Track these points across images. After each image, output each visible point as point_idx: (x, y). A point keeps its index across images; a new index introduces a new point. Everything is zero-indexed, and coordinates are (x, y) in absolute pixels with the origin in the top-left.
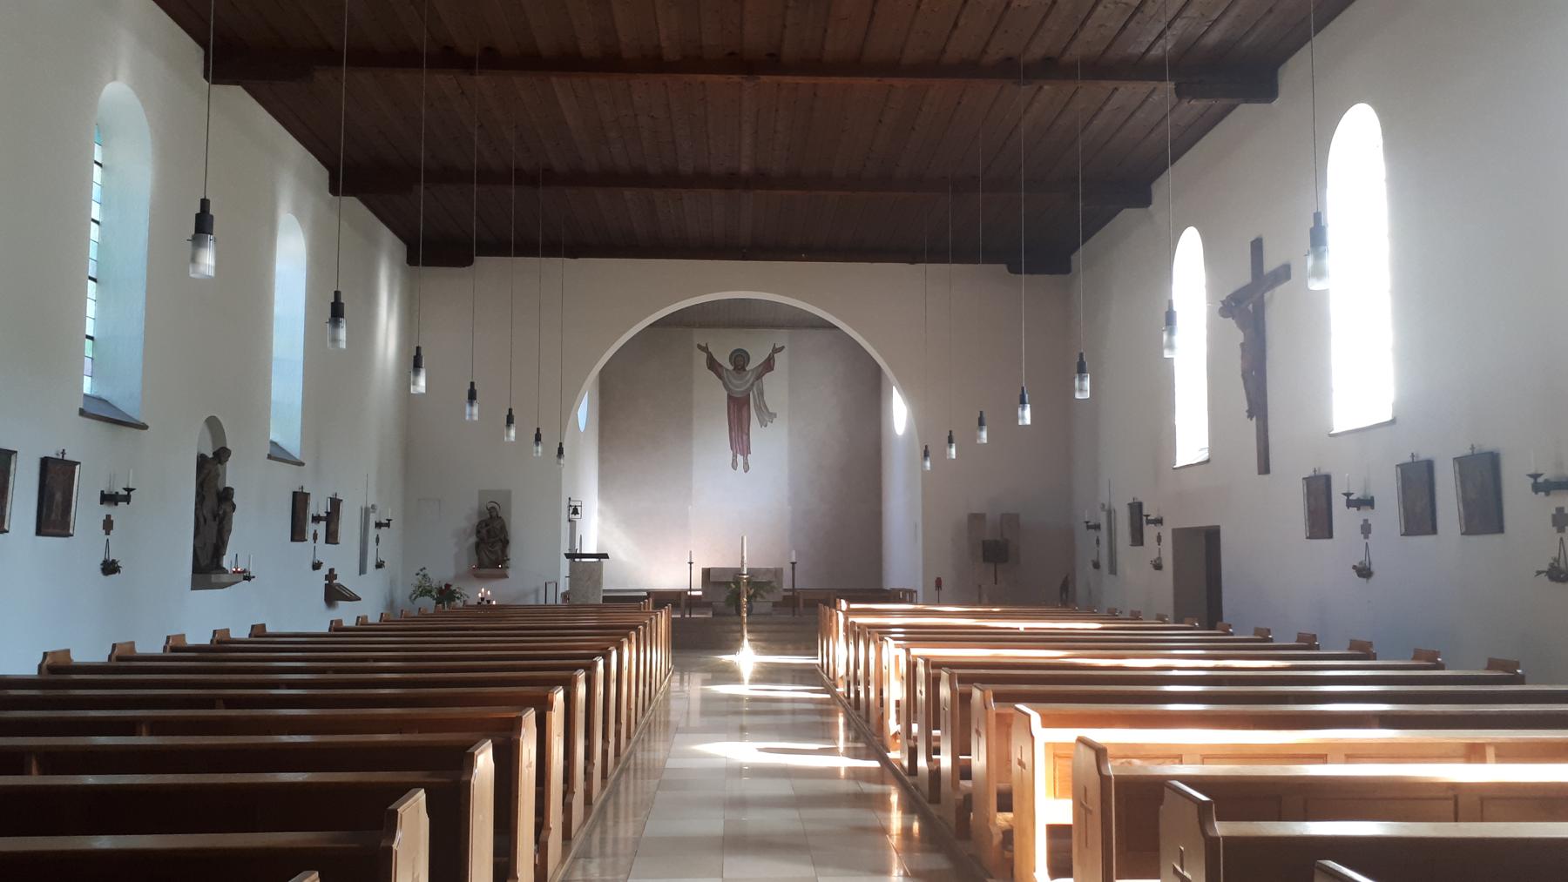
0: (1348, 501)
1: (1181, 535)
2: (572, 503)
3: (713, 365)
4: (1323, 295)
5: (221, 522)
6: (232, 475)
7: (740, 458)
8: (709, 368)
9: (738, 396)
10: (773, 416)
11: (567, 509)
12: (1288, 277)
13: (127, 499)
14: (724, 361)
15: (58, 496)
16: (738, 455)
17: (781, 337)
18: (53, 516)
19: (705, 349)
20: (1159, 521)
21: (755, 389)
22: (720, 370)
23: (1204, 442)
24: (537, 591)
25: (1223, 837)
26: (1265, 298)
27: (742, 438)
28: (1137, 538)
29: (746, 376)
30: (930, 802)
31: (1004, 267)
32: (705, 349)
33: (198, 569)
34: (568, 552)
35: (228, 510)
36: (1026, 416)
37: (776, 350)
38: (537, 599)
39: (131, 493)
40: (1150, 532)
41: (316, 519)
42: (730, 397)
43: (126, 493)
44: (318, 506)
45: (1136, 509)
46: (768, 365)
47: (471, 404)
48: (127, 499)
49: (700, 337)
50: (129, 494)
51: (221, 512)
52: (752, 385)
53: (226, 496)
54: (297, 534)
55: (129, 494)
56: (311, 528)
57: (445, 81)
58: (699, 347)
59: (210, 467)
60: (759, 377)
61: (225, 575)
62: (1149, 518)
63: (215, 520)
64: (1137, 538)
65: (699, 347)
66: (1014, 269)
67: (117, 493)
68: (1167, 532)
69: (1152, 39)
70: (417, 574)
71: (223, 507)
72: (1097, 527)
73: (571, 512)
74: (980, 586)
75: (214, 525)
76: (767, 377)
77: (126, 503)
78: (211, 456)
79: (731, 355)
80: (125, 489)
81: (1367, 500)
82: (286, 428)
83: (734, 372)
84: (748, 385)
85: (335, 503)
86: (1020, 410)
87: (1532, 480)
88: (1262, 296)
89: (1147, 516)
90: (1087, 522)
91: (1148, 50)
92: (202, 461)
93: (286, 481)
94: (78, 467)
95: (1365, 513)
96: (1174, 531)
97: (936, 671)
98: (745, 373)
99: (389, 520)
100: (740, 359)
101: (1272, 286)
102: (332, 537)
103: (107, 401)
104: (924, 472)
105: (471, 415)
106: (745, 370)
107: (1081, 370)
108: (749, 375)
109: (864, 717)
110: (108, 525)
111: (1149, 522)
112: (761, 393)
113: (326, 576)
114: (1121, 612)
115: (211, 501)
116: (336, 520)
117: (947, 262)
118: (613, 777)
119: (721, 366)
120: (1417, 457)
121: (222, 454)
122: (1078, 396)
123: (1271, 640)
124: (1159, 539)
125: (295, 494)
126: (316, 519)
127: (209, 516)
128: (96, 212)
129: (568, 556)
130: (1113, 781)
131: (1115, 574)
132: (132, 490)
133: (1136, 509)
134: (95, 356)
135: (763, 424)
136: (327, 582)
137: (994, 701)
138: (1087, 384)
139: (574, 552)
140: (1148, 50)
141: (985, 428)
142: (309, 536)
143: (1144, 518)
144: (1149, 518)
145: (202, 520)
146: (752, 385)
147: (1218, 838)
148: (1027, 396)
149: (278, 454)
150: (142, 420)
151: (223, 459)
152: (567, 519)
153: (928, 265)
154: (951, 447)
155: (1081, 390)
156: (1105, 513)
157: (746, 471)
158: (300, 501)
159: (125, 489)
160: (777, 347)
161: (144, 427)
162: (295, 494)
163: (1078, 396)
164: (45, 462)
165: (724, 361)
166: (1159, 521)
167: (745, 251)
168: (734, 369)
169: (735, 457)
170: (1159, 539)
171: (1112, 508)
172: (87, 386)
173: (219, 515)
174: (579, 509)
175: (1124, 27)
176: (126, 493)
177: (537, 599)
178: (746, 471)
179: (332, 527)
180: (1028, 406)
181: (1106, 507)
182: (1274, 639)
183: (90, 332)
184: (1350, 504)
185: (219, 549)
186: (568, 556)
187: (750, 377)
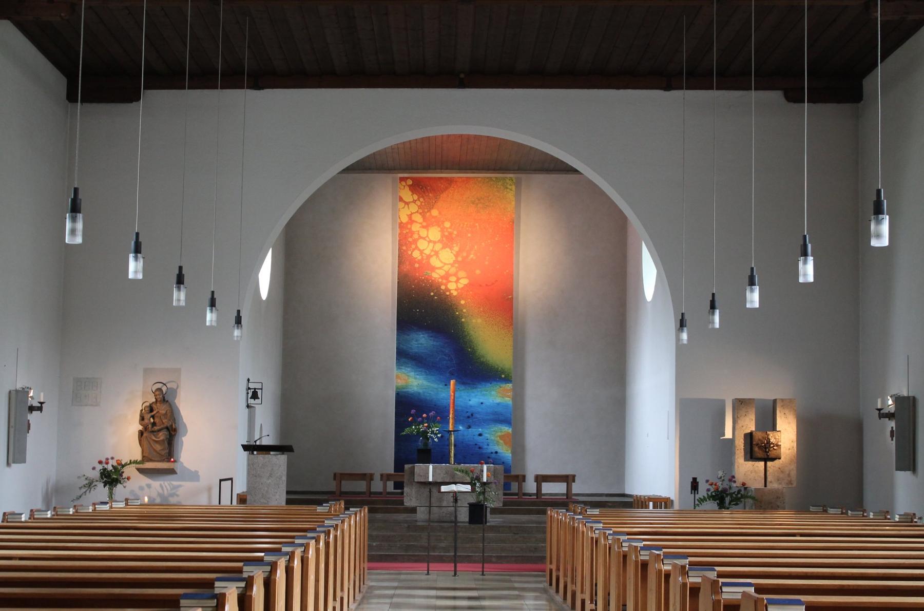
2: (251, 386)
4: (502, 368)
11: (245, 392)
24: (209, 489)
34: (246, 443)
36: (807, 271)
38: (210, 498)
39: (43, 405)
43: (40, 405)
47: (179, 289)
66: (794, 96)
70: (100, 462)
73: (250, 395)
74: (268, 435)
77: (40, 412)
86: (801, 264)
90: (879, 410)
99: (41, 403)
104: (257, 454)
105: (179, 300)
107: (878, 210)
117: (710, 88)
122: (874, 243)
132: (43, 403)
138: (885, 228)
139: (252, 443)
141: (757, 289)
148: (809, 246)
150: (260, 425)
152: (245, 405)
154: (713, 314)
163: (874, 243)
167: (462, 76)
174: (259, 392)
176: (40, 405)
177: (210, 498)
180: (810, 259)
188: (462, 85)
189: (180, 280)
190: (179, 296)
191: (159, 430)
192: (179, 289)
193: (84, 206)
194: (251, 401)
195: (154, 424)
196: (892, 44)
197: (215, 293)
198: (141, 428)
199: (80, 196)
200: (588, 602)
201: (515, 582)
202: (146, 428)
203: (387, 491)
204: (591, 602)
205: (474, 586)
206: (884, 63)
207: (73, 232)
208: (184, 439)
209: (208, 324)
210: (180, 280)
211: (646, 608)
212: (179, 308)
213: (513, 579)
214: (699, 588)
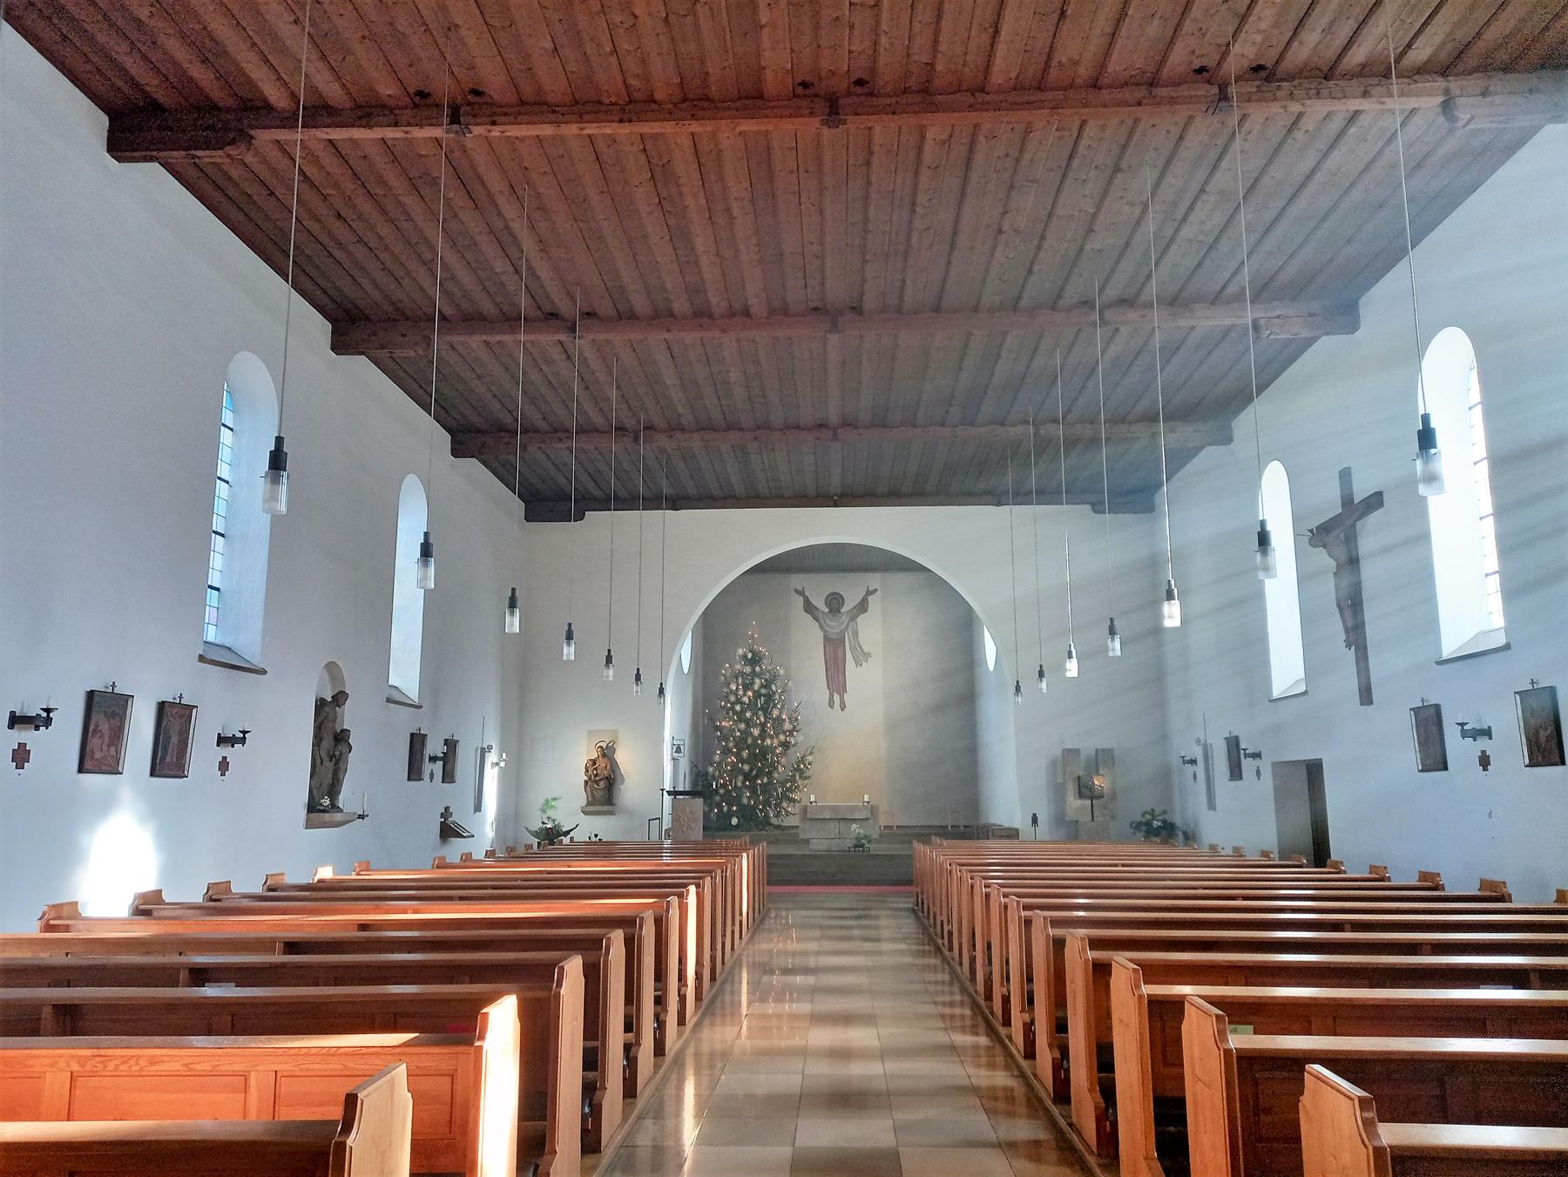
0: (1462, 730)
1: (1282, 768)
3: (809, 608)
5: (337, 763)
6: (350, 718)
7: (837, 698)
8: (806, 611)
9: (835, 637)
10: (867, 656)
12: (1381, 504)
13: (243, 741)
14: (819, 603)
15: (174, 739)
16: (835, 694)
17: (874, 580)
18: (168, 759)
19: (801, 593)
20: (1257, 755)
21: (850, 630)
22: (816, 612)
23: (1300, 673)
25: (1391, 1147)
26: (1357, 527)
27: (838, 677)
28: (1236, 772)
29: (841, 617)
30: (1026, 1057)
31: (1087, 508)
32: (801, 593)
33: (313, 807)
35: (344, 751)
37: (869, 593)
40: (1248, 765)
41: (433, 759)
42: (825, 638)
44: (434, 747)
45: (1233, 744)
46: (862, 607)
48: (243, 741)
49: (797, 581)
50: (48, 716)
51: (337, 753)
52: (848, 625)
53: (342, 738)
54: (414, 772)
55: (48, 716)
56: (428, 767)
57: (549, 339)
58: (796, 591)
59: (327, 710)
60: (853, 619)
61: (339, 814)
62: (1247, 752)
63: (331, 761)
64: (1236, 772)
65: (796, 591)
66: (1097, 508)
67: (234, 735)
68: (1266, 766)
69: (1227, 276)
71: (340, 748)
72: (1193, 762)
73: (675, 749)
75: (329, 765)
76: (861, 619)
78: (329, 699)
79: (829, 595)
80: (240, 731)
81: (1484, 730)
82: (405, 674)
83: (830, 615)
84: (844, 625)
85: (451, 745)
87: (1460, 727)
88: (1354, 525)
89: (1244, 750)
91: (1224, 288)
92: (321, 705)
93: (405, 724)
94: (195, 710)
95: (1482, 744)
96: (1274, 764)
97: (1028, 913)
98: (840, 615)
100: (835, 602)
101: (1363, 515)
102: (448, 776)
103: (229, 649)
105: (568, 654)
106: (840, 612)
108: (844, 617)
109: (958, 960)
110: (224, 766)
111: (1246, 756)
112: (856, 634)
113: (442, 814)
114: (1223, 849)
115: (327, 743)
116: (452, 760)
118: (693, 1023)
119: (817, 609)
120: (1537, 683)
121: (340, 698)
123: (1345, 872)
124: (1258, 773)
125: (412, 735)
126: (433, 759)
127: (325, 758)
128: (224, 470)
129: (669, 793)
130: (1235, 1056)
131: (1215, 810)
133: (1233, 744)
134: (220, 606)
135: (858, 664)
136: (443, 820)
137: (1090, 950)
140: (1224, 288)
142: (426, 776)
143: (1242, 752)
144: (1247, 752)
145: (319, 761)
146: (848, 625)
147: (1384, 1149)
149: (395, 700)
151: (340, 702)
153: (1013, 507)
155: (1170, 617)
156: (1201, 748)
157: (842, 710)
158: (417, 742)
159: (240, 731)
160: (870, 589)
161: (265, 672)
162: (412, 735)
164: (162, 706)
165: (819, 603)
166: (1257, 755)
167: (835, 498)
168: (830, 612)
169: (831, 696)
170: (1258, 773)
171: (1208, 742)
172: (211, 634)
173: (335, 756)
175: (1199, 265)
176: (242, 735)
178: (842, 710)
179: (448, 767)
181: (1202, 742)
182: (1392, 878)
183: (214, 579)
184: (1464, 734)
185: (333, 790)
186: (669, 793)
187: (845, 618)
188: (836, 505)
189: (569, 637)
190: (569, 650)
191: (601, 780)
192: (569, 645)
193: (435, 550)
194: (675, 755)
195: (596, 775)
196: (1260, 390)
197: (573, 626)
198: (586, 778)
199: (517, 594)
200: (945, 924)
201: (889, 902)
202: (590, 778)
203: (1252, 1026)
204: (948, 924)
205: (855, 907)
206: (1259, 398)
207: (512, 625)
208: (622, 787)
209: (564, 658)
210: (569, 637)
211: (23, 1023)
212: (569, 661)
213: (888, 899)
214: (1065, 940)
